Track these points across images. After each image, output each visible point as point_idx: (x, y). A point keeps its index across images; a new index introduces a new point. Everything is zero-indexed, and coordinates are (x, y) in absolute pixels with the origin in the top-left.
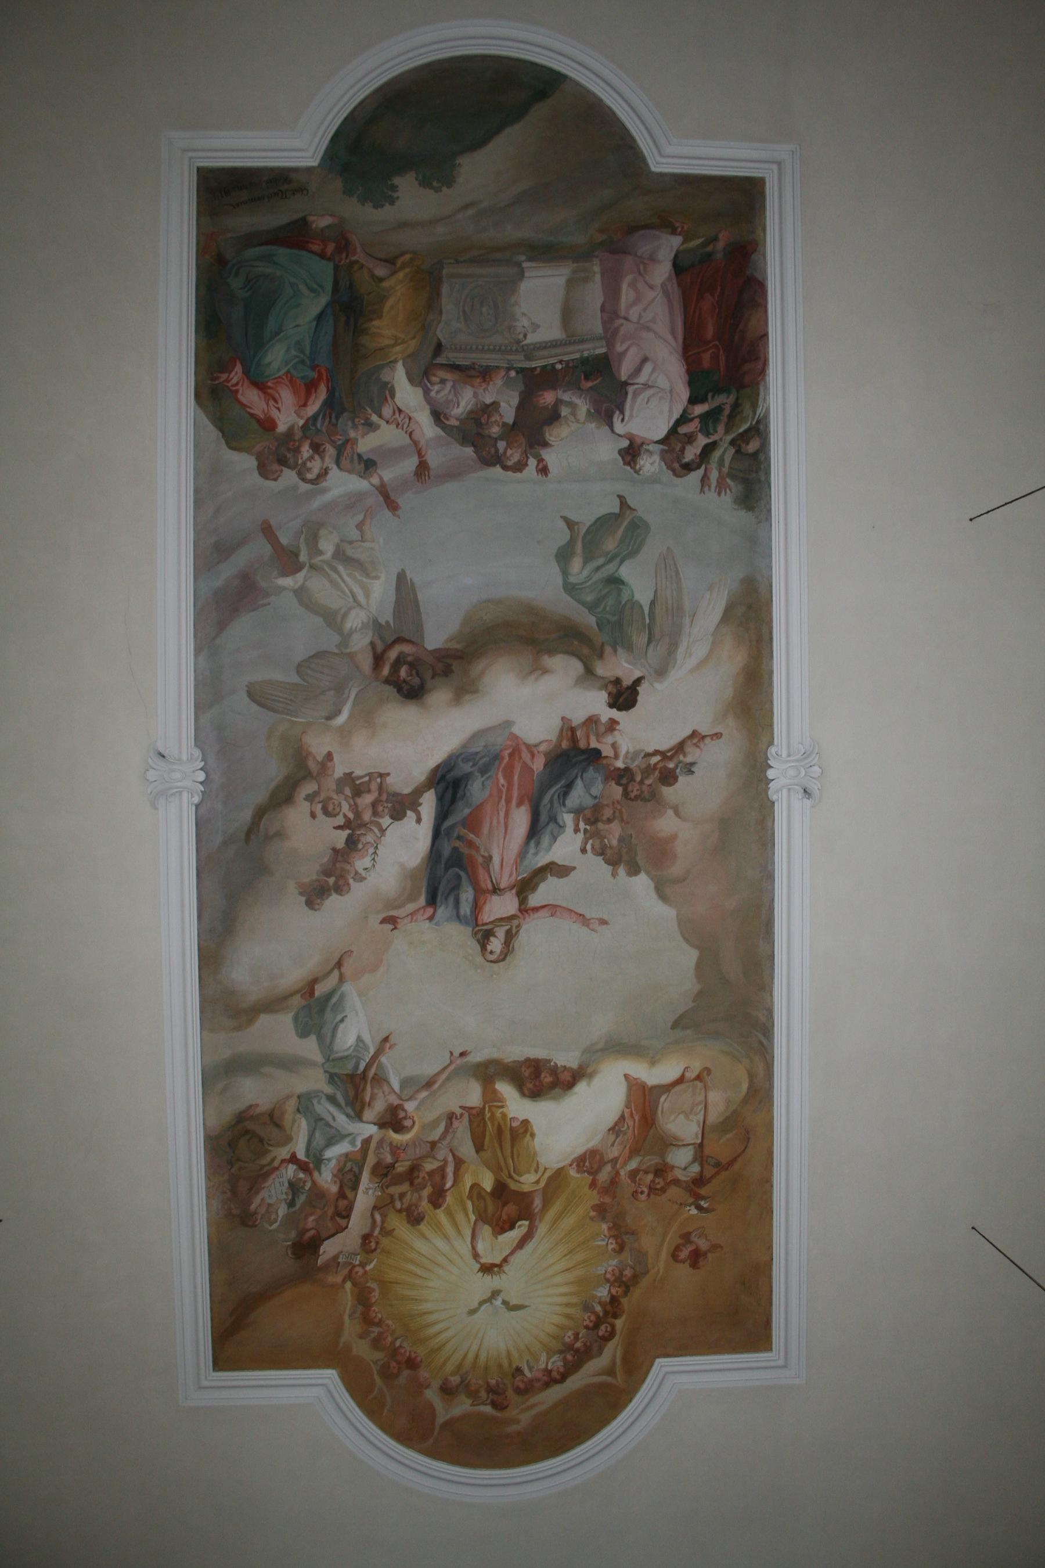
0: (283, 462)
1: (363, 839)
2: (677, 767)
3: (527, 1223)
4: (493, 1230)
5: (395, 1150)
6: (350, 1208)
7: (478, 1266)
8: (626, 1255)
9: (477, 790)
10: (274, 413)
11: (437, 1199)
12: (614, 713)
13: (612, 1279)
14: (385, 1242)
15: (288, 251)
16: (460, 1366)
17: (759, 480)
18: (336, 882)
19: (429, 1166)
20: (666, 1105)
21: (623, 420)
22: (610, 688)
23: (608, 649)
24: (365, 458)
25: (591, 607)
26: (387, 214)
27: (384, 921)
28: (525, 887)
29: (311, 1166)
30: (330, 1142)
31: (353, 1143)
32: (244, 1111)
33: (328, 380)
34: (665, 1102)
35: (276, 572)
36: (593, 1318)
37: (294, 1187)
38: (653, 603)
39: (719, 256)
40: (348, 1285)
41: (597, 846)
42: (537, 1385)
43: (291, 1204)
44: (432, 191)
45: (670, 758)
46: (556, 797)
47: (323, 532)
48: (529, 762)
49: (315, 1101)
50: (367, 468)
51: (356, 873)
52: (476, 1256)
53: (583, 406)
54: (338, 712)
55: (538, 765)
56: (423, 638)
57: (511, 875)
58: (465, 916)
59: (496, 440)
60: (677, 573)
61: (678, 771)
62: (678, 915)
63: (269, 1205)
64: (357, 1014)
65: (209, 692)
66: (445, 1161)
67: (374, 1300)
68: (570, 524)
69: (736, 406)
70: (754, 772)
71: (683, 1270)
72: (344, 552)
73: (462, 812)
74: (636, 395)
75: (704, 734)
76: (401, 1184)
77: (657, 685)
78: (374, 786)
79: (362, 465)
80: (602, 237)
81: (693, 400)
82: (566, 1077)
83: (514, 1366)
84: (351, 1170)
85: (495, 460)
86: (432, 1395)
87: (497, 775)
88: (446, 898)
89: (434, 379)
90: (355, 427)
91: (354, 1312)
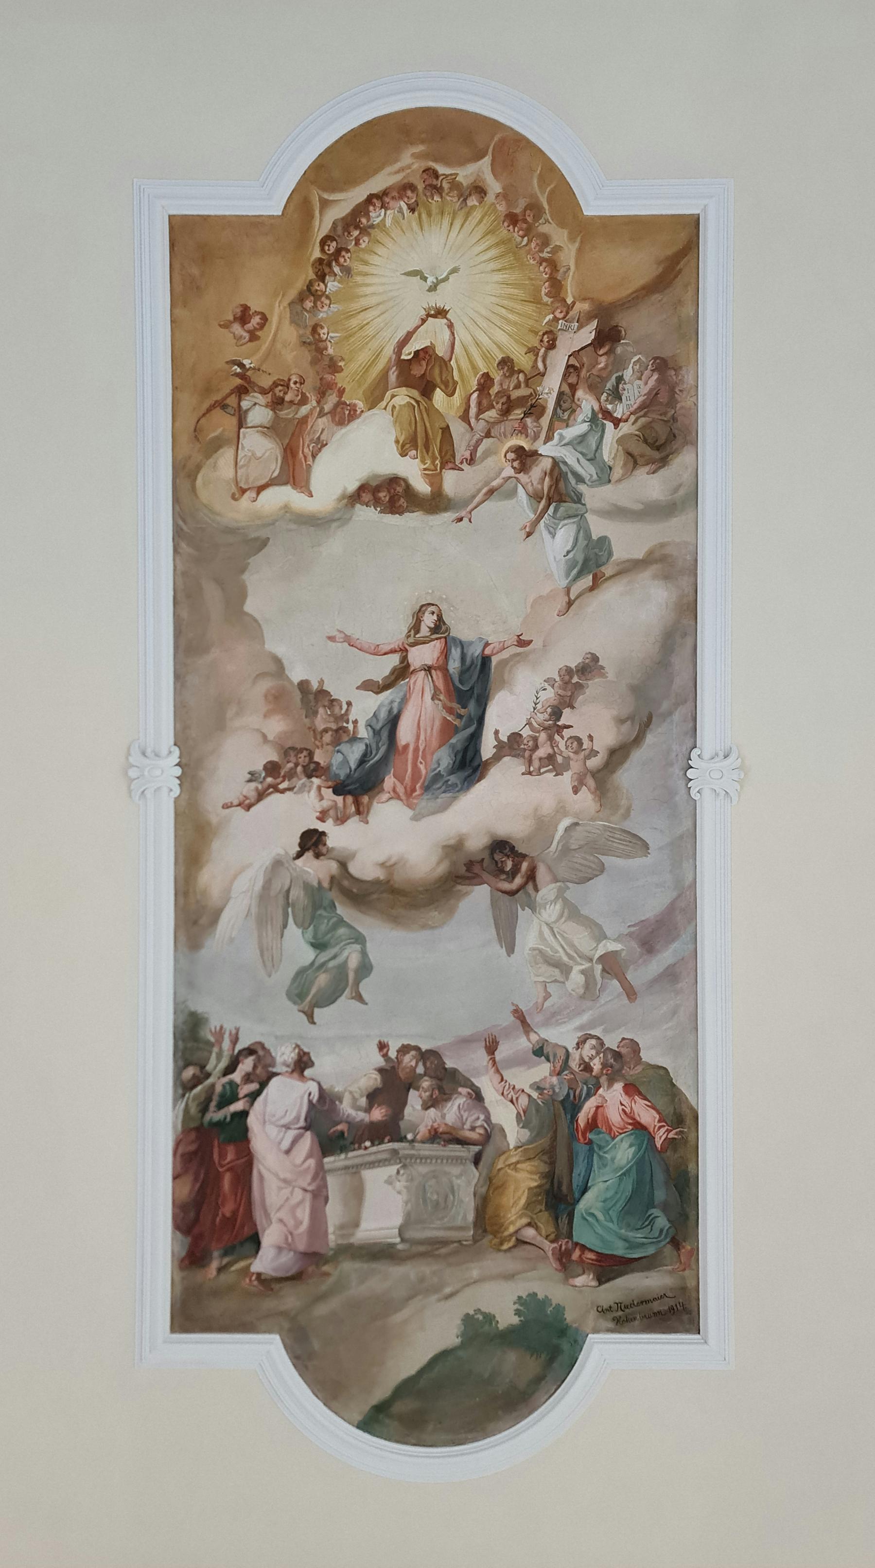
0: (617, 1055)
1: (547, 716)
2: (264, 778)
3: (403, 357)
4: (434, 351)
5: (523, 430)
6: (566, 376)
7: (448, 316)
8: (310, 323)
9: (444, 759)
10: (626, 1100)
11: (486, 382)
12: (320, 827)
13: (323, 299)
14: (534, 342)
15: (615, 1253)
16: (468, 215)
17: (183, 1040)
18: (571, 678)
19: (492, 414)
20: (273, 467)
21: (310, 1094)
22: (324, 850)
23: (326, 884)
24: (543, 1058)
25: (341, 922)
26: (523, 1288)
27: (529, 642)
28: (402, 672)
29: (600, 416)
30: (582, 439)
31: (562, 437)
32: (660, 468)
33: (577, 1129)
34: (274, 469)
35: (623, 955)
36: (342, 260)
37: (616, 395)
38: (285, 926)
39: (216, 1254)
40: (569, 300)
41: (337, 710)
42: (395, 194)
43: (620, 379)
44: (483, 1310)
45: (270, 786)
46: (374, 752)
47: (581, 991)
48: (398, 784)
49: (595, 477)
50: (542, 1048)
51: (553, 686)
52: (451, 326)
53: (346, 1108)
54: (567, 830)
55: (389, 781)
56: (492, 896)
57: (415, 683)
58: (456, 646)
59: (425, 1074)
60: (262, 955)
61: (263, 775)
62: (264, 644)
63: (640, 379)
64: (555, 558)
65: (685, 845)
66: (477, 418)
67: (547, 284)
68: (359, 998)
69: (204, 1109)
70: (191, 773)
71: (255, 305)
72: (562, 973)
73: (457, 740)
74: (297, 1119)
75: (239, 808)
76: (518, 398)
77: (282, 852)
78: (536, 763)
79: (545, 1052)
80: (326, 1268)
81: (244, 1114)
82: (366, 497)
83: (416, 213)
84: (564, 411)
85: (425, 1056)
86: (494, 186)
87: (427, 773)
88: (472, 662)
89: (482, 1131)
90: (552, 1087)
91: (565, 272)
